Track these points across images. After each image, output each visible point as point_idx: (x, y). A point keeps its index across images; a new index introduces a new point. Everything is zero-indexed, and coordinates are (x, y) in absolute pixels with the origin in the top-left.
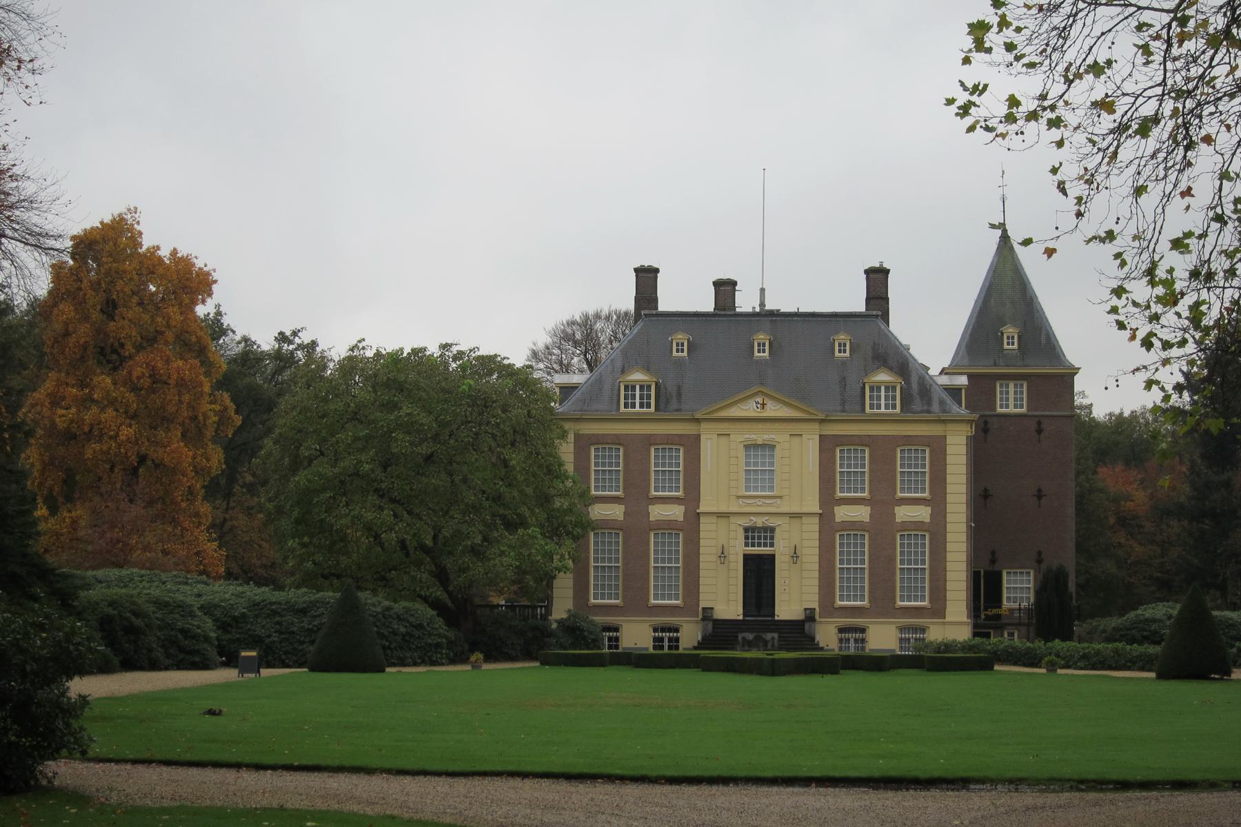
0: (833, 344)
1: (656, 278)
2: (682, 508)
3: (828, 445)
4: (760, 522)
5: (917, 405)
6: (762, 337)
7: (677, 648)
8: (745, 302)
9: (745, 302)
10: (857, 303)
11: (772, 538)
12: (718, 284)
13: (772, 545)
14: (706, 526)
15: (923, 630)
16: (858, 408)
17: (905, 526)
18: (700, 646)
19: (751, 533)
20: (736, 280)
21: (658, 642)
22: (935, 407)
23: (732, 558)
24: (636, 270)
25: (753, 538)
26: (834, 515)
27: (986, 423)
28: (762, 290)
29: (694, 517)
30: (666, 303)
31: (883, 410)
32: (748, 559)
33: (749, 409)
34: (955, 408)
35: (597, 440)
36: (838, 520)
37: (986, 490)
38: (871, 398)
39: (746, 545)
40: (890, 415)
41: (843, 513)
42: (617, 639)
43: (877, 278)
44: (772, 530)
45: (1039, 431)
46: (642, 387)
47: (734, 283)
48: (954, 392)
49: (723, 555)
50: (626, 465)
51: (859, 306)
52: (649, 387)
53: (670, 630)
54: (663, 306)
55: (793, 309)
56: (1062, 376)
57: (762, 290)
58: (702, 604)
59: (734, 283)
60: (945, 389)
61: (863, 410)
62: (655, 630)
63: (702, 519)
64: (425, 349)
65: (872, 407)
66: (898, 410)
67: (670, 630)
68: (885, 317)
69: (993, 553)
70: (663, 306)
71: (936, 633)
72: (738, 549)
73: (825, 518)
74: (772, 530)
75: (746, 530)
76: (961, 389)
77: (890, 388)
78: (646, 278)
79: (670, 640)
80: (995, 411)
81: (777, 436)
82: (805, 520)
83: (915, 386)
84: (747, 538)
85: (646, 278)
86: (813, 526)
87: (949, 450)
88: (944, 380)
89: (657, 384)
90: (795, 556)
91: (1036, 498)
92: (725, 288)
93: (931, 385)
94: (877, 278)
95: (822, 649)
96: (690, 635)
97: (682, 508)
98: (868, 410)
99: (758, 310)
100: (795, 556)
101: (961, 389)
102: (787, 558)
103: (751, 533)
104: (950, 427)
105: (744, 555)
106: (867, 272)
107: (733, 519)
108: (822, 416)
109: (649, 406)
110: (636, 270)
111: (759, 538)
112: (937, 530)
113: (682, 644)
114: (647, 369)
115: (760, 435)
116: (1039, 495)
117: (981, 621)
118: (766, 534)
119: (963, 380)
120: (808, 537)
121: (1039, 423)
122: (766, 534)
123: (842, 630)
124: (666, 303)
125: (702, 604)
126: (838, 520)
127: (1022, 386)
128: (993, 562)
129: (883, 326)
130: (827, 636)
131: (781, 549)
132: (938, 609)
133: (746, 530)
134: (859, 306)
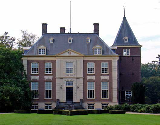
0: (86, 40)
1: (47, 26)
2: (52, 77)
3: (85, 62)
4: (70, 80)
5: (106, 53)
6: (71, 38)
7: (94, 109)
8: (67, 31)
9: (67, 31)
10: (91, 31)
11: (73, 83)
12: (61, 28)
13: (73, 85)
14: (57, 80)
15: (107, 104)
16: (92, 54)
17: (103, 80)
18: (56, 108)
19: (67, 82)
20: (46, 23)
21: (47, 108)
22: (110, 54)
23: (63, 88)
24: (60, 28)
25: (68, 83)
26: (87, 78)
27: (121, 58)
28: (70, 29)
29: (54, 79)
30: (49, 31)
31: (98, 54)
32: (67, 88)
33: (67, 54)
34: (114, 53)
35: (33, 61)
36: (101, 79)
37: (121, 73)
38: (95, 51)
39: (67, 85)
40: (96, 55)
41: (88, 78)
42: (37, 107)
43: (96, 26)
44: (73, 81)
45: (133, 60)
46: (43, 49)
47: (65, 28)
48: (114, 50)
49: (61, 88)
50: (39, 67)
51: (92, 32)
52: (44, 49)
53: (106, 104)
54: (48, 32)
55: (77, 32)
56: (138, 48)
57: (70, 29)
58: (57, 99)
59: (65, 28)
60: (112, 50)
61: (93, 54)
62: (46, 105)
63: (56, 79)
64: (148, 63)
65: (95, 53)
66: (101, 54)
67: (106, 104)
68: (98, 34)
69: (123, 87)
70: (48, 32)
71: (110, 104)
72: (65, 86)
73: (85, 78)
74: (73, 81)
75: (67, 81)
76: (115, 50)
77: (99, 49)
78: (45, 26)
79: (49, 107)
80: (123, 55)
81: (74, 60)
82: (80, 79)
83: (105, 49)
84: (67, 83)
85: (45, 26)
86: (82, 80)
87: (113, 63)
88: (112, 48)
89: (46, 49)
90: (78, 88)
91: (132, 75)
92: (63, 29)
93: (109, 49)
94: (96, 26)
95: (84, 109)
96: (54, 105)
97: (52, 77)
98: (94, 54)
99: (69, 33)
100: (78, 88)
101: (115, 50)
102: (76, 88)
103: (67, 82)
104: (113, 58)
105: (66, 87)
106: (94, 24)
107: (63, 79)
108: (84, 55)
109: (44, 53)
110: (60, 28)
111: (70, 83)
112: (110, 81)
113: (95, 108)
114: (44, 45)
115: (69, 60)
116: (133, 74)
117: (120, 102)
118: (72, 82)
119: (116, 48)
120: (81, 83)
121: (133, 58)
122: (72, 82)
123: (89, 104)
124: (49, 31)
125: (57, 99)
126: (101, 79)
127: (129, 50)
128: (123, 89)
129: (97, 35)
130: (85, 105)
131: (74, 86)
132: (111, 100)
133: (67, 81)
134: (92, 32)
